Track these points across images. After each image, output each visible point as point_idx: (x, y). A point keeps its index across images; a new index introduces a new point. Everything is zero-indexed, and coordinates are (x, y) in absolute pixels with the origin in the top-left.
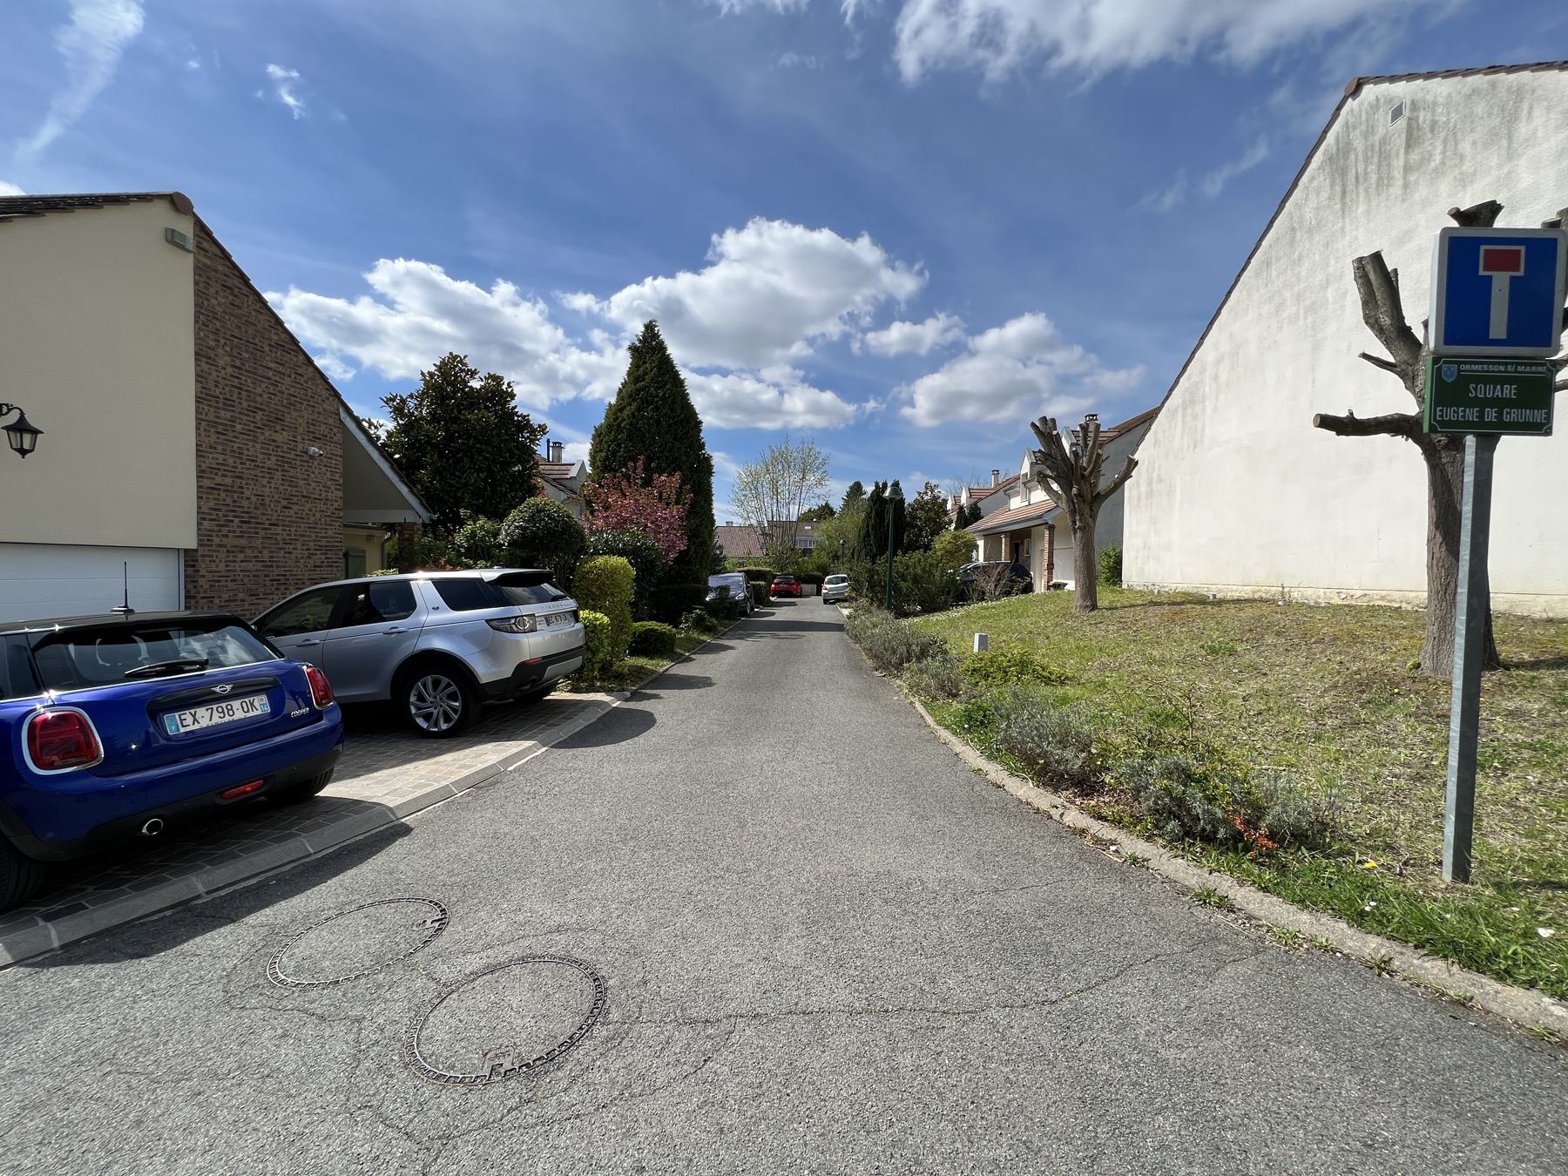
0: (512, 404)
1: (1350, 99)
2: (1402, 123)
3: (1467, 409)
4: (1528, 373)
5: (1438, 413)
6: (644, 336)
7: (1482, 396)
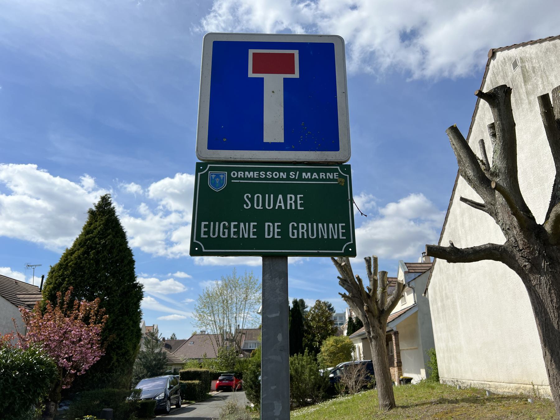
0: (65, 252)
1: (492, 60)
2: (518, 69)
3: (242, 225)
4: (315, 179)
5: (203, 229)
6: (99, 204)
7: (260, 208)
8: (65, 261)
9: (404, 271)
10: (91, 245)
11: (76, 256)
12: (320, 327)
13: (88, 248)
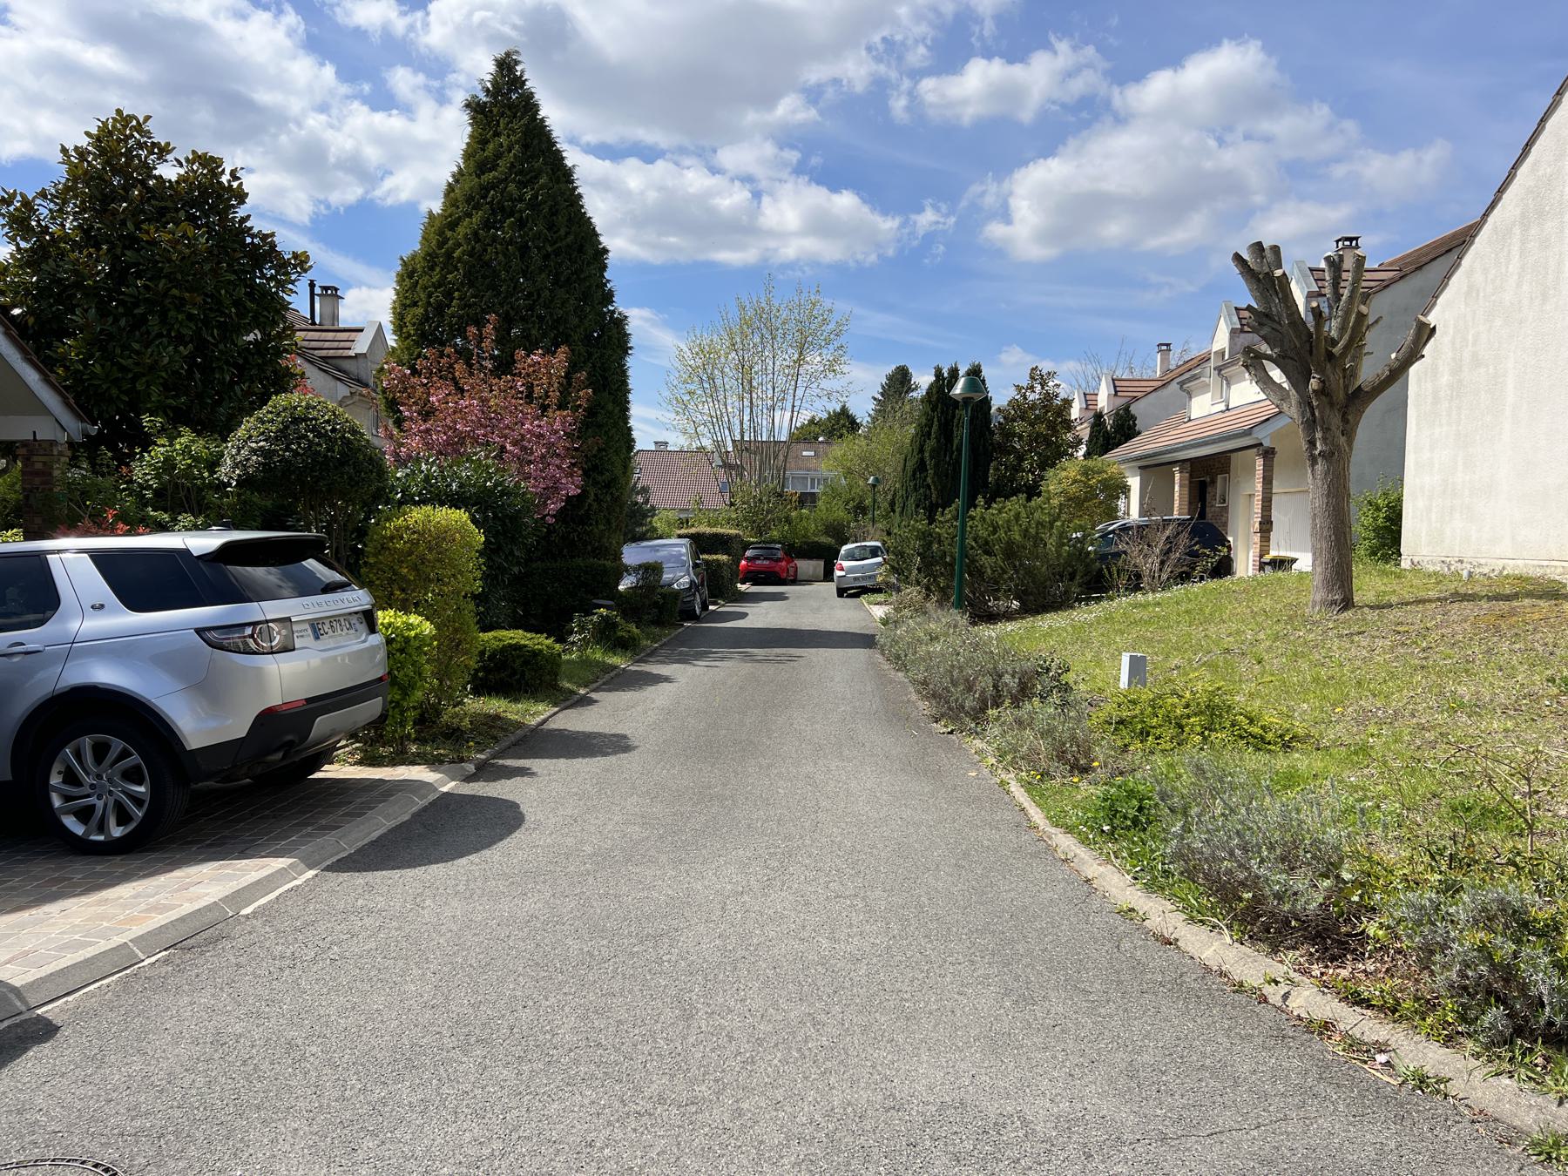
0: (241, 212)
6: (495, 83)
8: (441, 245)
9: (1306, 291)
10: (498, 203)
11: (468, 231)
12: (1039, 435)
13: (494, 213)
